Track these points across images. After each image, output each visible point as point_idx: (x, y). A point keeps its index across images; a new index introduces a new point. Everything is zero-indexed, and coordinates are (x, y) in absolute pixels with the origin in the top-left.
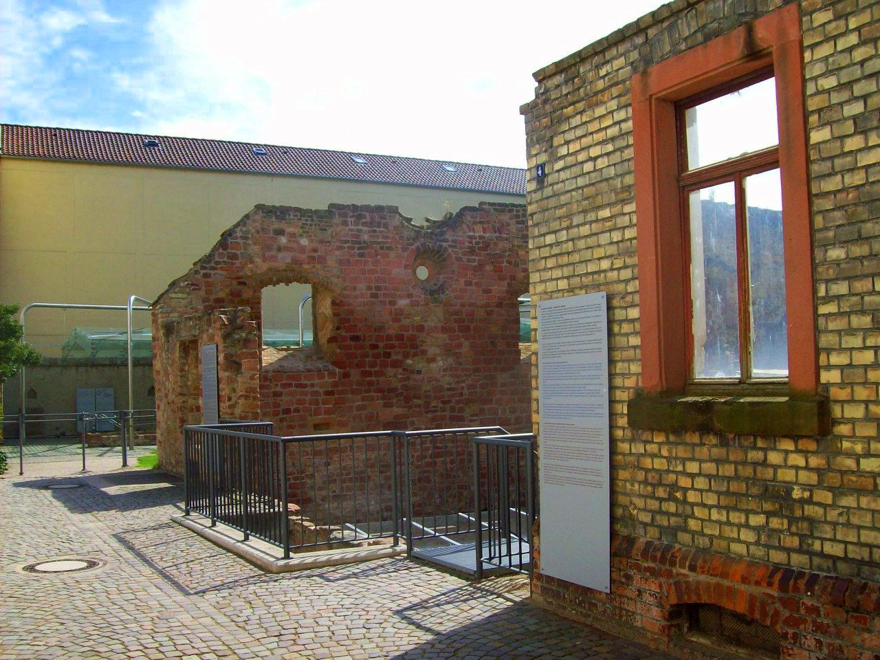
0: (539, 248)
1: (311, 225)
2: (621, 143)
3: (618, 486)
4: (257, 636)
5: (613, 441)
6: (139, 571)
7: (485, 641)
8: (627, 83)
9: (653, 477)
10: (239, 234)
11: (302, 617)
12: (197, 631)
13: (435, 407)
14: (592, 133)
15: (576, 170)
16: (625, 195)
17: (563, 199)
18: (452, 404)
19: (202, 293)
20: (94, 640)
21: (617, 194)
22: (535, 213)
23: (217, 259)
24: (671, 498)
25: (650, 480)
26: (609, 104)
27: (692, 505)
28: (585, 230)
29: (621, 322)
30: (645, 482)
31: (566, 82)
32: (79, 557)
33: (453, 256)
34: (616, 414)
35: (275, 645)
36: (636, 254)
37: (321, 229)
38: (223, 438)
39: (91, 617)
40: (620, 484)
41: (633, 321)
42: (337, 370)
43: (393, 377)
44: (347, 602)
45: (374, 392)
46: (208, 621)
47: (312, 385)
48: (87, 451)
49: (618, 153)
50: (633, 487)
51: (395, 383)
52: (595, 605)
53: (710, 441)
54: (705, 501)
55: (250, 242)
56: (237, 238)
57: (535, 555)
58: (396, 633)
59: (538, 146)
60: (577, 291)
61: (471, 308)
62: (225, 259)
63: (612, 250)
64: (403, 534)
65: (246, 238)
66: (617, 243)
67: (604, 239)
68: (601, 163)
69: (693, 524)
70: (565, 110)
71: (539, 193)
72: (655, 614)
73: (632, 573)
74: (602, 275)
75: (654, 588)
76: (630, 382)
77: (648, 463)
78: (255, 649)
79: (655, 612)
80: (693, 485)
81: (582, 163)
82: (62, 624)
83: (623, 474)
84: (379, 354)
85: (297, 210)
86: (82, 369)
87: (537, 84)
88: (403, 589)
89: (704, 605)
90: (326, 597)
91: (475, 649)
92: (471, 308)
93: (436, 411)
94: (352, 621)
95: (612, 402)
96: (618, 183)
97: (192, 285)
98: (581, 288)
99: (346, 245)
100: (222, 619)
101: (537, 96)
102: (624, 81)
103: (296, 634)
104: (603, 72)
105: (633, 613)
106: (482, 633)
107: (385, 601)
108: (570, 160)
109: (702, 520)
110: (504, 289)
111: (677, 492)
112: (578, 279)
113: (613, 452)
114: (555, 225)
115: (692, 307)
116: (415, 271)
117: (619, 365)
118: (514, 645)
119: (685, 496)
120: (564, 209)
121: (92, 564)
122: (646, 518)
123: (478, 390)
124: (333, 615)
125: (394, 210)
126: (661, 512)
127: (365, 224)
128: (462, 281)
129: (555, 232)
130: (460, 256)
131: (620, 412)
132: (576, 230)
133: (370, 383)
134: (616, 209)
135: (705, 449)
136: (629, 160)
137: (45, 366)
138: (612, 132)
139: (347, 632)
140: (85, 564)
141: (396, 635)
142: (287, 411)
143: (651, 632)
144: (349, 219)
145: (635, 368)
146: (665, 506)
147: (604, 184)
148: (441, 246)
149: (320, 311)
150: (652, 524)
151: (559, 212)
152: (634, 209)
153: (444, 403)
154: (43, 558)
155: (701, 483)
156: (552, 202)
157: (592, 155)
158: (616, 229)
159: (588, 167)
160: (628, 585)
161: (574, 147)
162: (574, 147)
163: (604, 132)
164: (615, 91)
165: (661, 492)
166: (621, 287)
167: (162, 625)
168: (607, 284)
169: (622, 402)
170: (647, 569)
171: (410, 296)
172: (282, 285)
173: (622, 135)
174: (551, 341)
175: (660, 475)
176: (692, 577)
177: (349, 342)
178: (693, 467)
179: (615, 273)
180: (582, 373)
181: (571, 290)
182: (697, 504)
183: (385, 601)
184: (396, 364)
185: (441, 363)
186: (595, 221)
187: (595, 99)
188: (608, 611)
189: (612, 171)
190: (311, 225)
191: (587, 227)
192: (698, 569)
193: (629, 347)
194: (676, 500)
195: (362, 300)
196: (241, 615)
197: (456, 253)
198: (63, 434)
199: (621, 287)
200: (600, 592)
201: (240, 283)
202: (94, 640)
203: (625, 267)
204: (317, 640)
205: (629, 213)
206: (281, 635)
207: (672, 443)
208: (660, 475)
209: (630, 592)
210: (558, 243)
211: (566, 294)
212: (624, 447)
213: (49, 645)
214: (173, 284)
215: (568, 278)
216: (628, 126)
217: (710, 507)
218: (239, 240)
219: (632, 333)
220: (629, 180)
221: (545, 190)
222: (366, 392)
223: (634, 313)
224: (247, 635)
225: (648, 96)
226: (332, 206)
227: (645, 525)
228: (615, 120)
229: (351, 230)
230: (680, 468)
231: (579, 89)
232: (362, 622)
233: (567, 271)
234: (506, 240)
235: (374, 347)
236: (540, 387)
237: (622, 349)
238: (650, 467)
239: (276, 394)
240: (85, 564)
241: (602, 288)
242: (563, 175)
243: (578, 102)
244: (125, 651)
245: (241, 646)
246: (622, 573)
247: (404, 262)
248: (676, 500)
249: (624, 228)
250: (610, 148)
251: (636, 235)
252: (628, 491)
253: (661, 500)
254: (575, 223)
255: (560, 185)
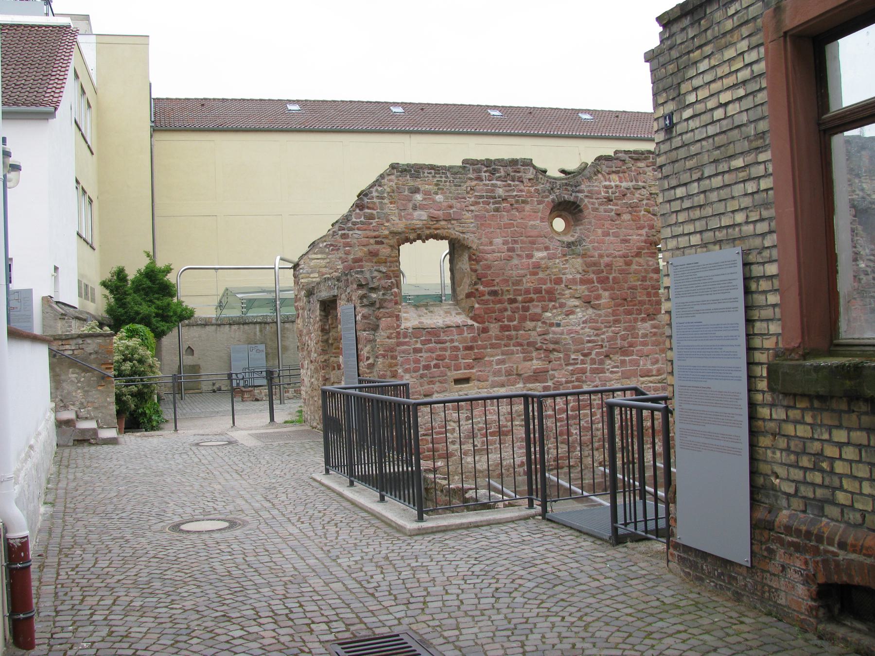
0: (669, 201)
1: (445, 182)
2: (753, 86)
3: (758, 453)
4: (386, 604)
5: (752, 406)
6: (277, 532)
7: (616, 614)
8: (759, 20)
9: (796, 445)
10: (375, 194)
11: (431, 584)
12: (327, 597)
13: (574, 359)
14: (721, 78)
15: (706, 118)
16: (759, 143)
17: (694, 149)
18: (593, 356)
19: (341, 254)
20: (228, 605)
21: (750, 142)
22: (664, 165)
23: (354, 220)
24: (816, 468)
25: (792, 449)
26: (739, 46)
27: (841, 476)
28: (717, 182)
29: (758, 278)
30: (788, 450)
31: (692, 24)
32: (219, 516)
33: (590, 206)
34: (755, 377)
35: (402, 614)
36: (773, 206)
37: (456, 186)
38: (358, 398)
39: (227, 580)
40: (761, 451)
41: (771, 277)
42: (476, 324)
43: (533, 331)
44: (476, 569)
45: (514, 346)
46: (337, 586)
47: (452, 341)
48: (238, 407)
49: (750, 98)
50: (775, 457)
51: (534, 336)
52: (735, 579)
53: (860, 408)
54: (855, 473)
55: (386, 201)
56: (373, 197)
57: (671, 522)
58: (526, 603)
59: (664, 95)
60: (711, 247)
61: (610, 259)
62: (362, 219)
63: (747, 202)
64: (537, 496)
65: (383, 198)
66: (753, 194)
67: (738, 190)
68: (732, 109)
69: (842, 497)
70: (692, 55)
71: (668, 144)
72: (800, 592)
73: (774, 547)
74: (737, 229)
75: (799, 564)
76: (769, 343)
77: (789, 429)
78: (382, 618)
79: (801, 590)
80: (841, 455)
81: (712, 110)
82: (199, 587)
83: (764, 441)
84: (518, 308)
85: (432, 167)
86: (235, 327)
87: (661, 29)
88: (535, 554)
89: (857, 587)
90: (456, 563)
91: (607, 624)
92: (610, 259)
93: (577, 364)
94: (481, 589)
95: (750, 364)
96: (751, 130)
97: (331, 245)
98: (715, 243)
99: (481, 200)
100: (352, 584)
101: (662, 42)
102: (755, 19)
103: (425, 603)
104: (731, 11)
105: (777, 590)
106: (614, 606)
107: (516, 568)
108: (700, 108)
109: (852, 493)
110: (643, 238)
111: (822, 462)
112: (711, 234)
113: (753, 417)
114: (685, 178)
115: (836, 261)
116: (551, 223)
117: (758, 325)
118: (650, 619)
119: (832, 468)
120: (695, 160)
121: (233, 524)
122: (789, 488)
123: (619, 341)
124: (463, 582)
125: (528, 163)
126: (805, 482)
127: (498, 179)
128: (600, 231)
129: (685, 184)
130: (597, 206)
131: (759, 375)
132: (707, 182)
133: (510, 338)
134: (750, 159)
135: (854, 416)
136: (762, 104)
137: (201, 325)
138: (745, 74)
139: (476, 601)
140: (226, 524)
141: (526, 606)
142: (427, 367)
143: (798, 612)
144: (483, 174)
145: (775, 328)
146: (810, 477)
147: (736, 131)
148: (577, 197)
149: (458, 267)
150: (796, 495)
151: (690, 164)
152: (770, 158)
153: (585, 355)
154: (186, 517)
155: (850, 453)
156: (682, 153)
157: (723, 101)
158: (750, 179)
159: (719, 114)
160: (770, 559)
161: (702, 94)
162: (702, 94)
163: (734, 76)
164: (745, 31)
165: (805, 462)
166: (757, 242)
167: (293, 590)
168: (742, 238)
169: (762, 364)
170: (791, 544)
171: (547, 248)
172: (419, 242)
173: (755, 77)
174: (685, 300)
175: (804, 443)
176: (842, 555)
177: (487, 297)
178: (840, 436)
179: (751, 227)
180: (718, 334)
181: (704, 245)
182: (846, 476)
183: (516, 568)
184: (535, 318)
185: (580, 315)
186: (727, 172)
187: (723, 41)
188: (749, 585)
189: (744, 118)
190: (445, 182)
191: (720, 178)
192: (849, 548)
193: (767, 306)
194: (822, 471)
195: (499, 254)
196: (371, 580)
197: (593, 204)
198: (219, 389)
199: (757, 242)
200: (741, 565)
201: (377, 243)
202: (228, 605)
203: (762, 220)
204: (445, 609)
205: (764, 162)
206: (410, 603)
207: (817, 409)
208: (804, 443)
209: (774, 567)
210: (690, 196)
211: (699, 250)
212: (764, 412)
213: (186, 608)
214: (313, 245)
215: (701, 232)
216: (760, 67)
217: (861, 480)
218: (375, 200)
219: (770, 291)
220: (763, 126)
221: (674, 140)
222: (505, 346)
223: (772, 269)
224: (376, 602)
225: (782, 34)
226: (465, 161)
227: (788, 495)
228: (747, 62)
229: (487, 185)
230: (826, 436)
231: (706, 30)
232: (490, 590)
233: (699, 225)
234: (644, 187)
235: (512, 301)
236: (674, 346)
237: (760, 307)
238: (793, 434)
239: (416, 351)
240: (226, 524)
241: (737, 242)
242: (692, 124)
243: (705, 44)
244: (255, 617)
245: (370, 614)
246: (764, 547)
247: (540, 214)
248: (822, 471)
249: (759, 178)
250: (741, 92)
251: (772, 186)
252: (769, 459)
253: (805, 469)
254: (706, 175)
255: (690, 135)
